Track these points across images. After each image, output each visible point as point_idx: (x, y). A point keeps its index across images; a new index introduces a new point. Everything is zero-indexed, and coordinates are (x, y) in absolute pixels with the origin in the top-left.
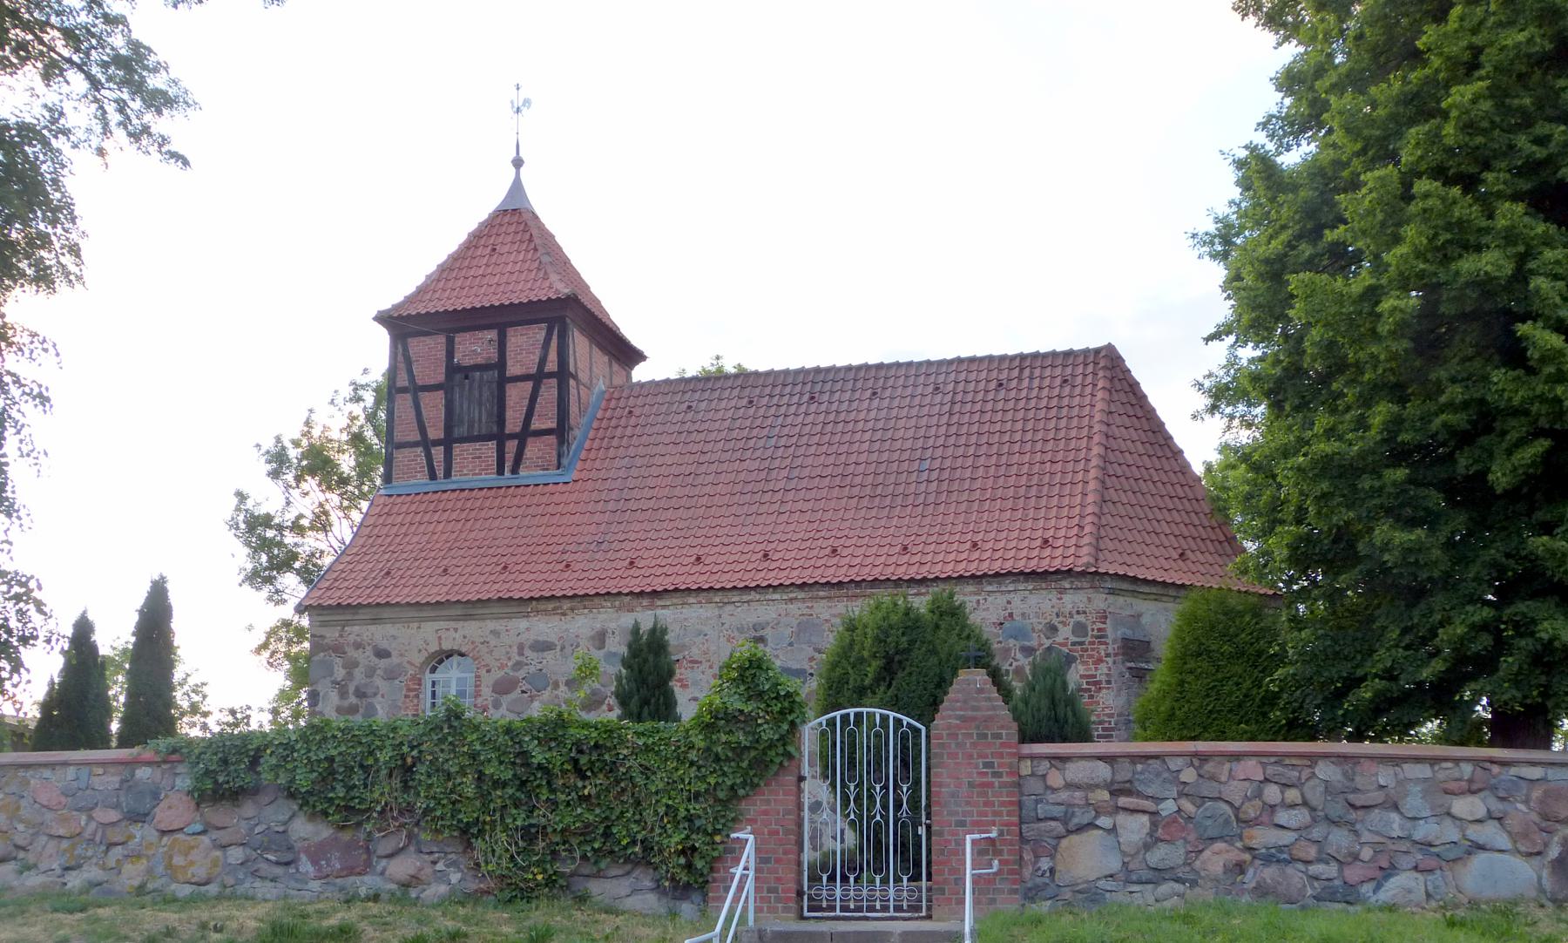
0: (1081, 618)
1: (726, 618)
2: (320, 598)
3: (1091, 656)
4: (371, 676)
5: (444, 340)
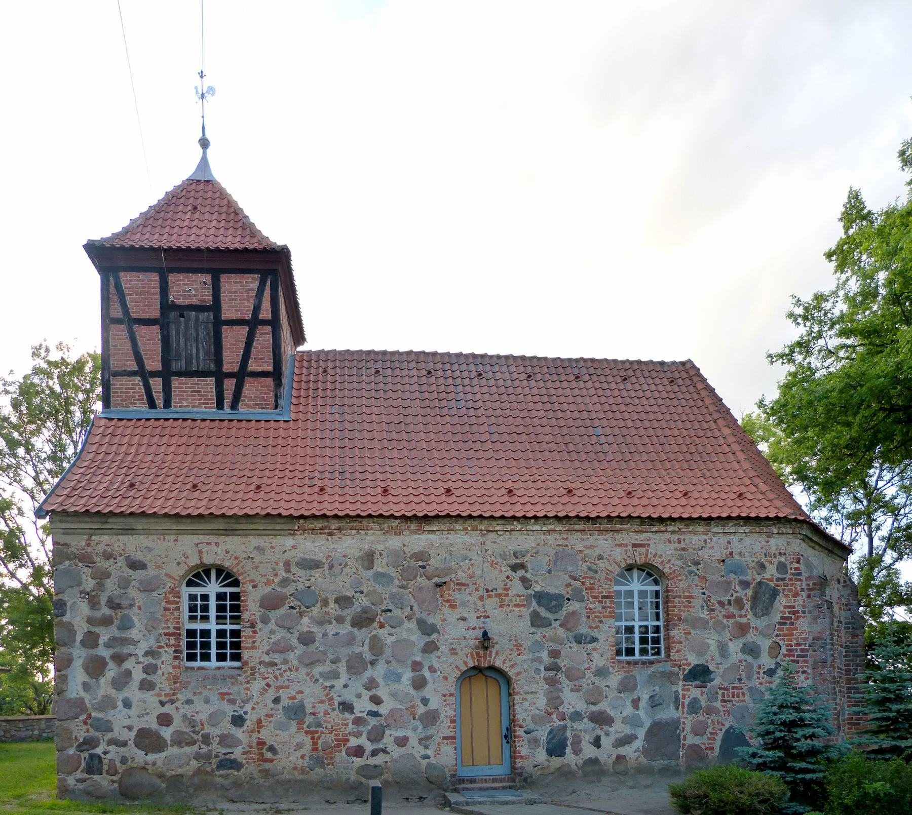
0: (782, 559)
1: (489, 545)
2: (61, 504)
3: (790, 590)
4: (126, 588)
5: (157, 278)
